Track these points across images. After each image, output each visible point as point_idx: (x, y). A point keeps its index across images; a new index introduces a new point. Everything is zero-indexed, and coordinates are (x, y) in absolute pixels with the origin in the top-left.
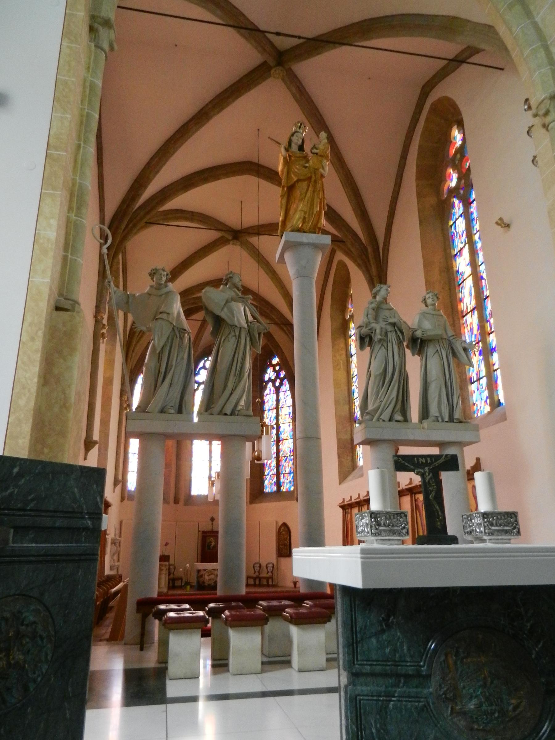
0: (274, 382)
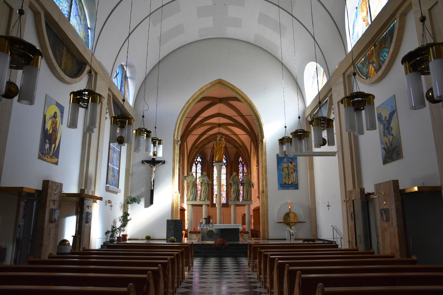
0: (242, 163)
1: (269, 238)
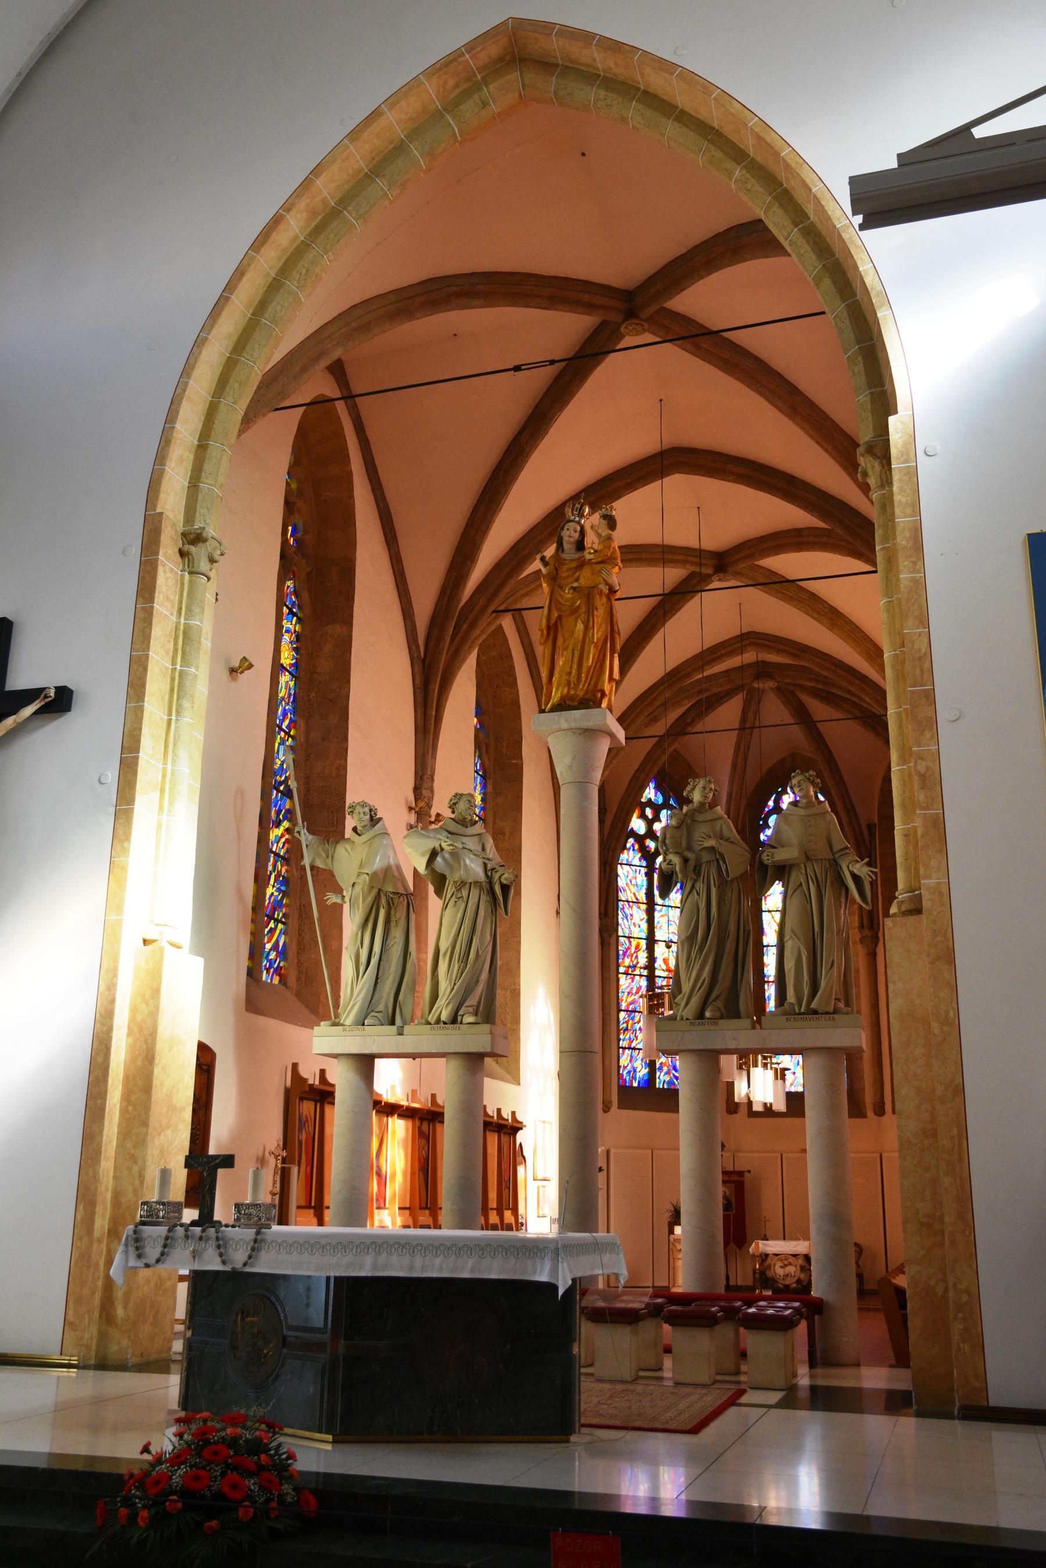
1: (995, 1400)
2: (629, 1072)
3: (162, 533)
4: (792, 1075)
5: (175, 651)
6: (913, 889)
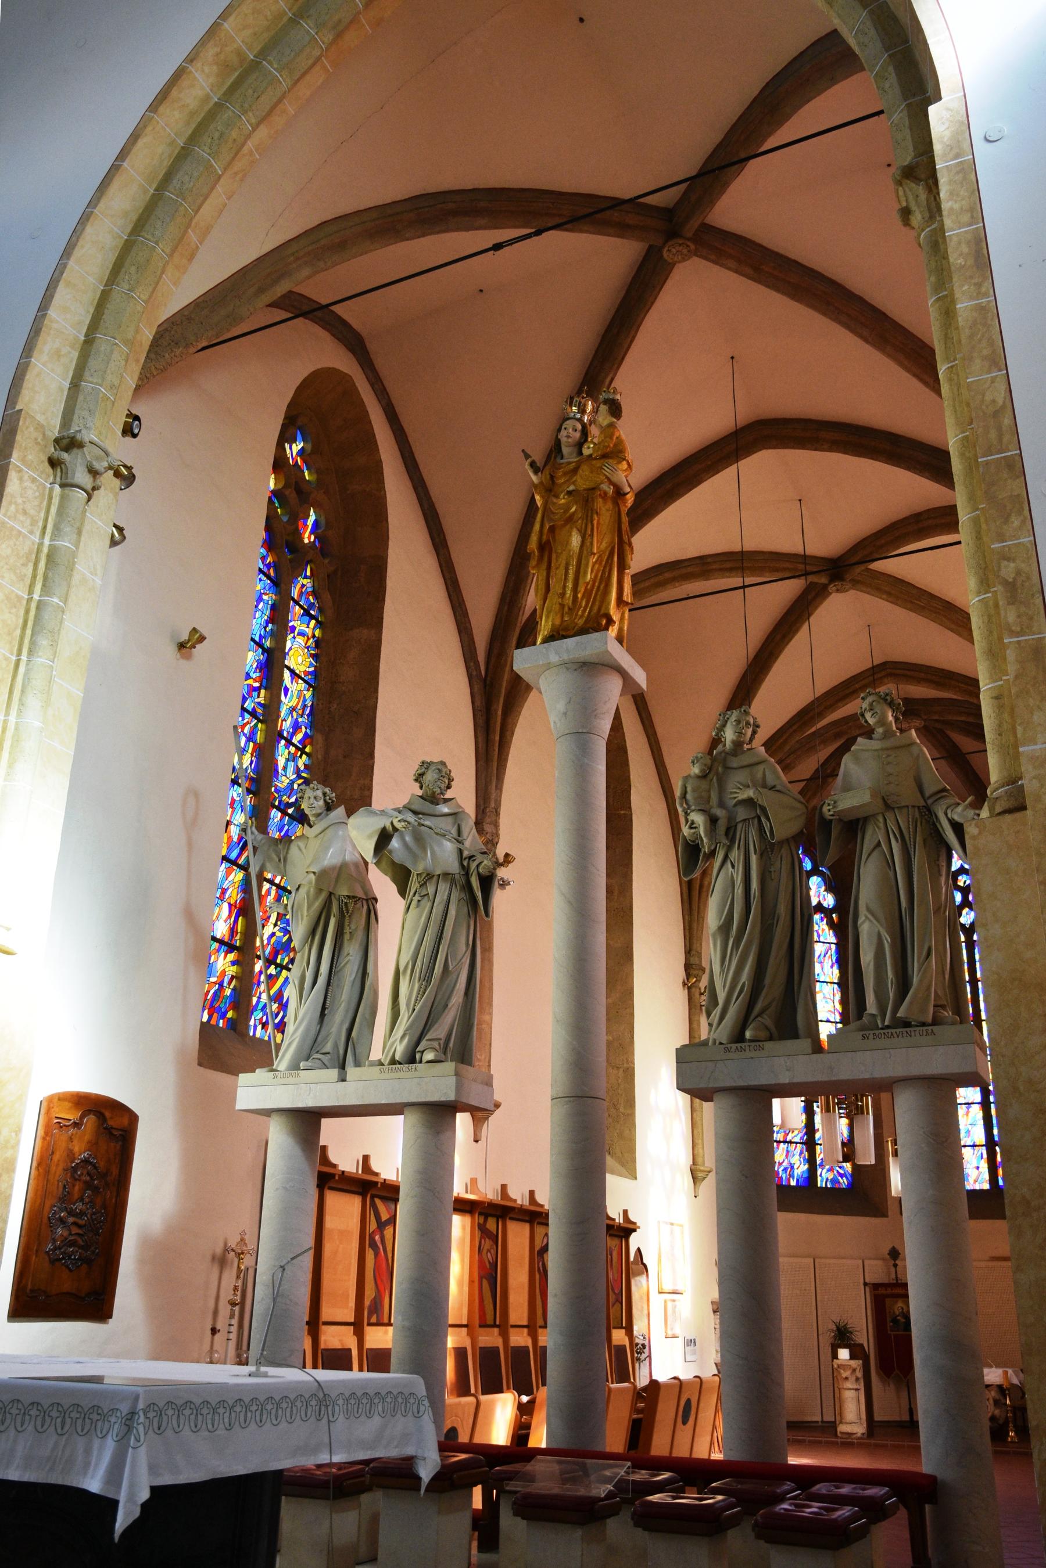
2: (785, 1169)
3: (19, 432)
4: (975, 1170)
5: (34, 577)
6: (1013, 780)
